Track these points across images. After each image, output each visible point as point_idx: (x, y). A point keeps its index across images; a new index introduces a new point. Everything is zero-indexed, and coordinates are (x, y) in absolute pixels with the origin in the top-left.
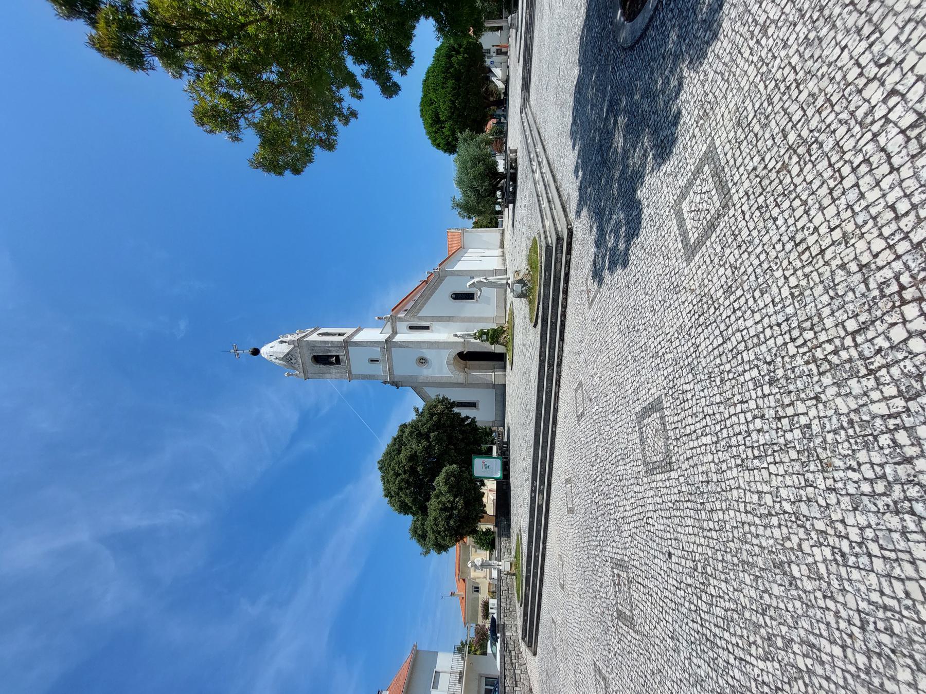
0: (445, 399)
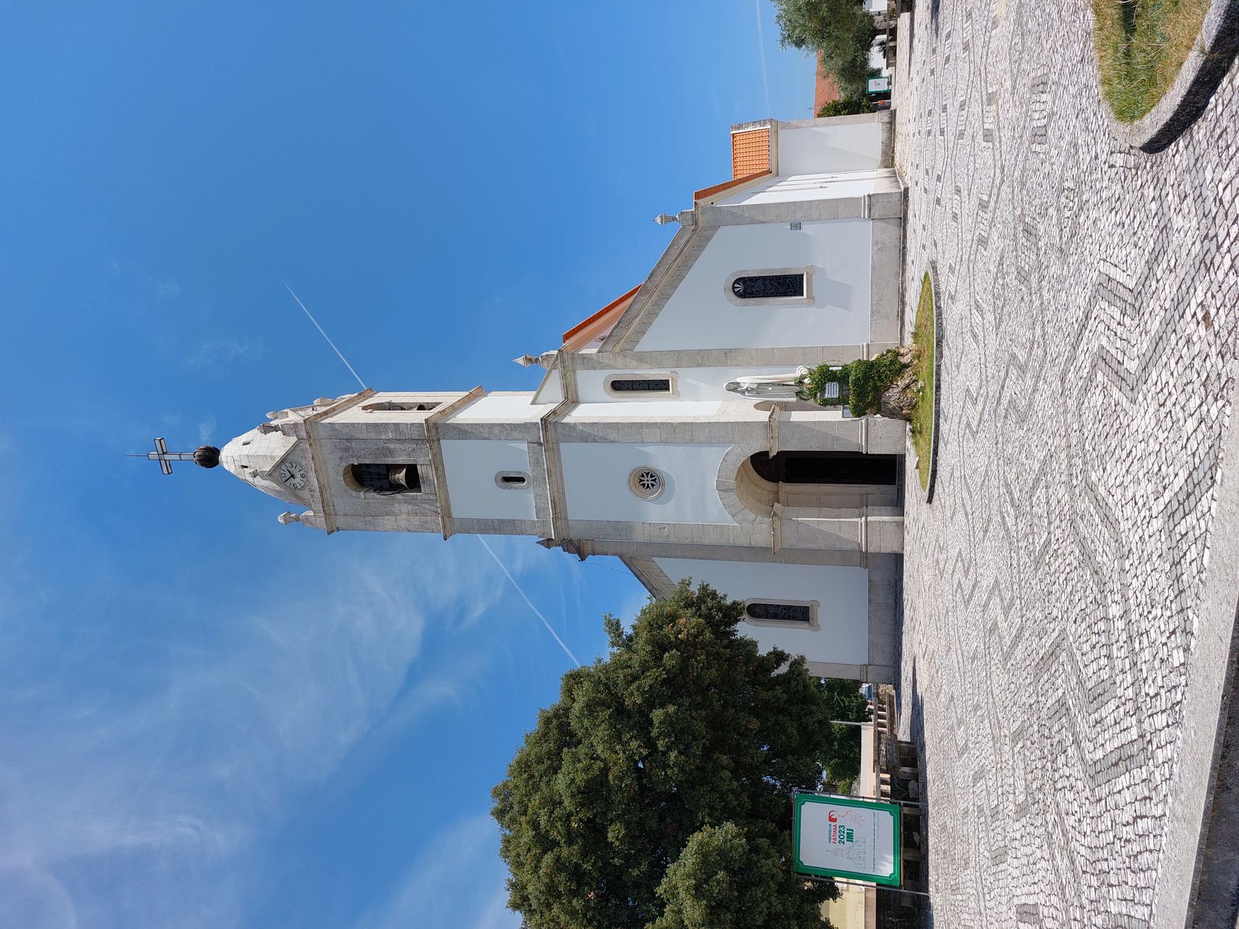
0: (707, 594)
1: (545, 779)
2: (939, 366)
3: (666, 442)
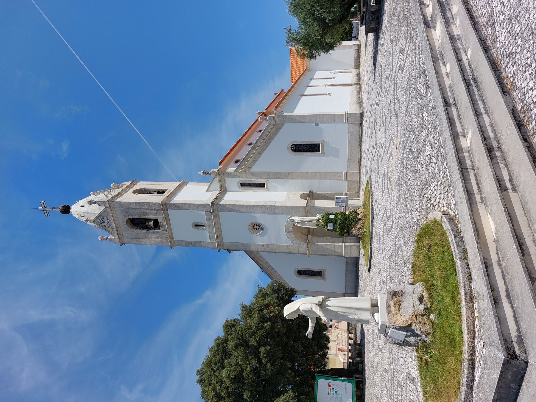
1: (218, 371)
2: (372, 230)
3: (264, 213)
